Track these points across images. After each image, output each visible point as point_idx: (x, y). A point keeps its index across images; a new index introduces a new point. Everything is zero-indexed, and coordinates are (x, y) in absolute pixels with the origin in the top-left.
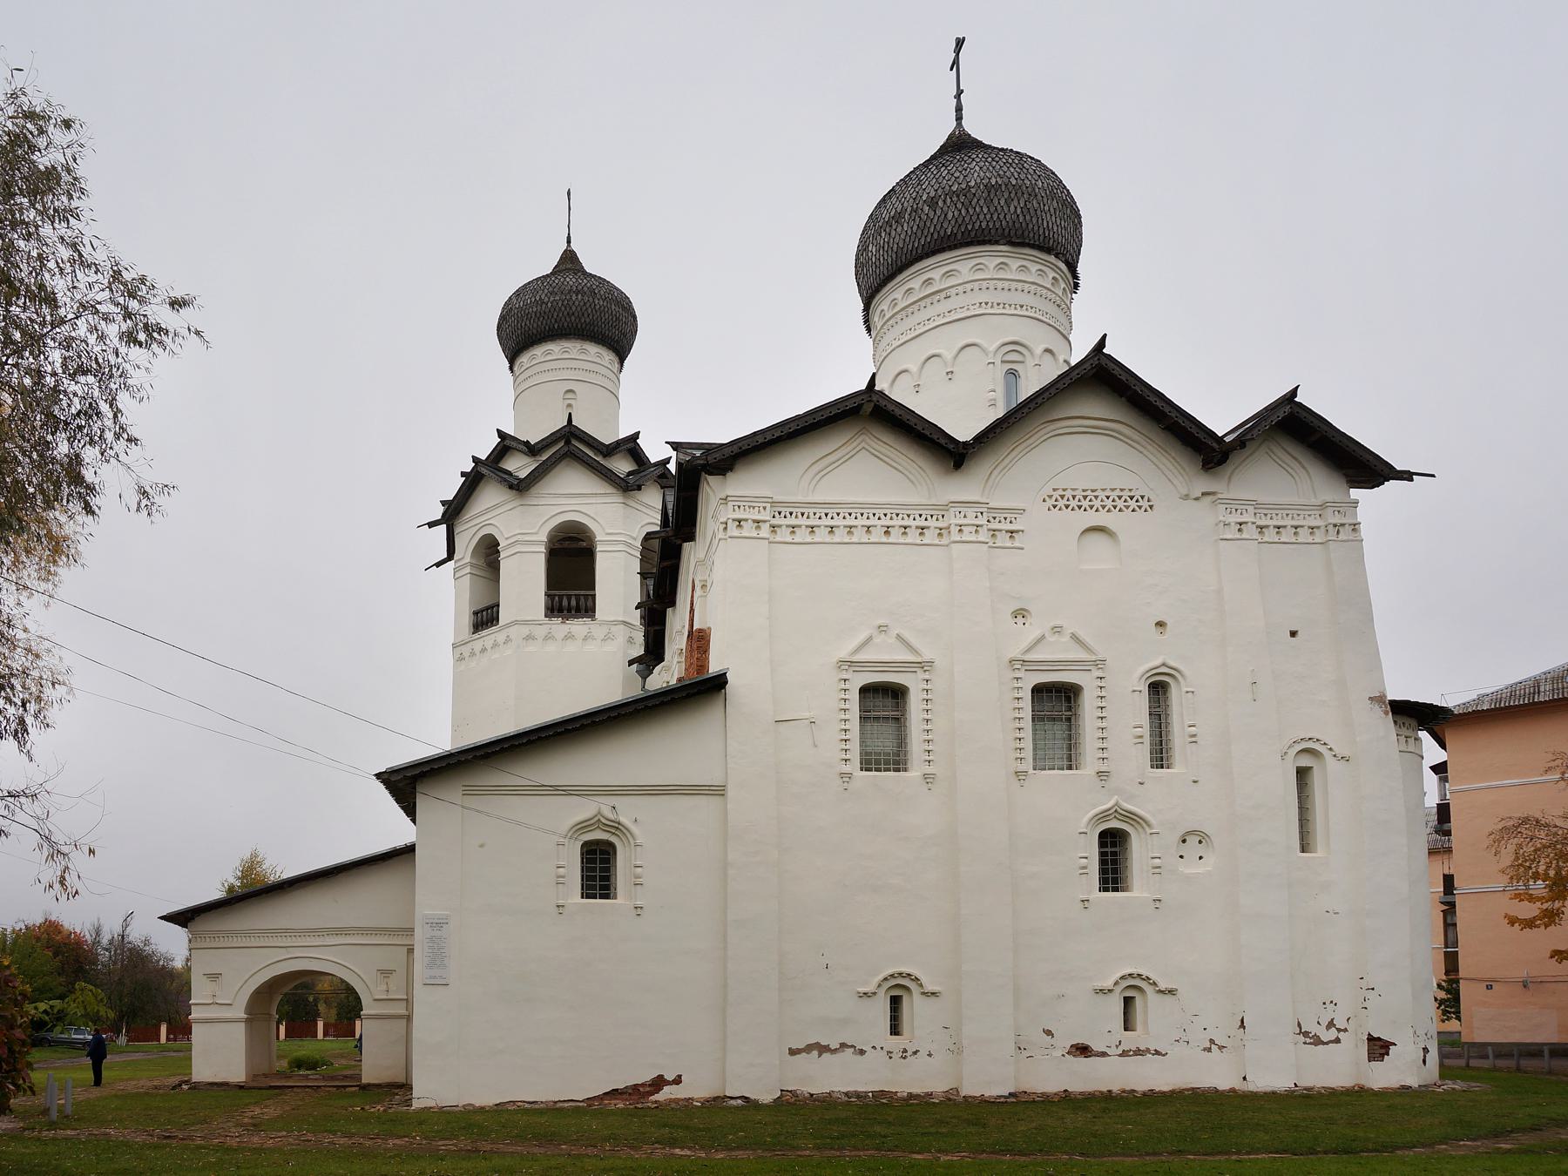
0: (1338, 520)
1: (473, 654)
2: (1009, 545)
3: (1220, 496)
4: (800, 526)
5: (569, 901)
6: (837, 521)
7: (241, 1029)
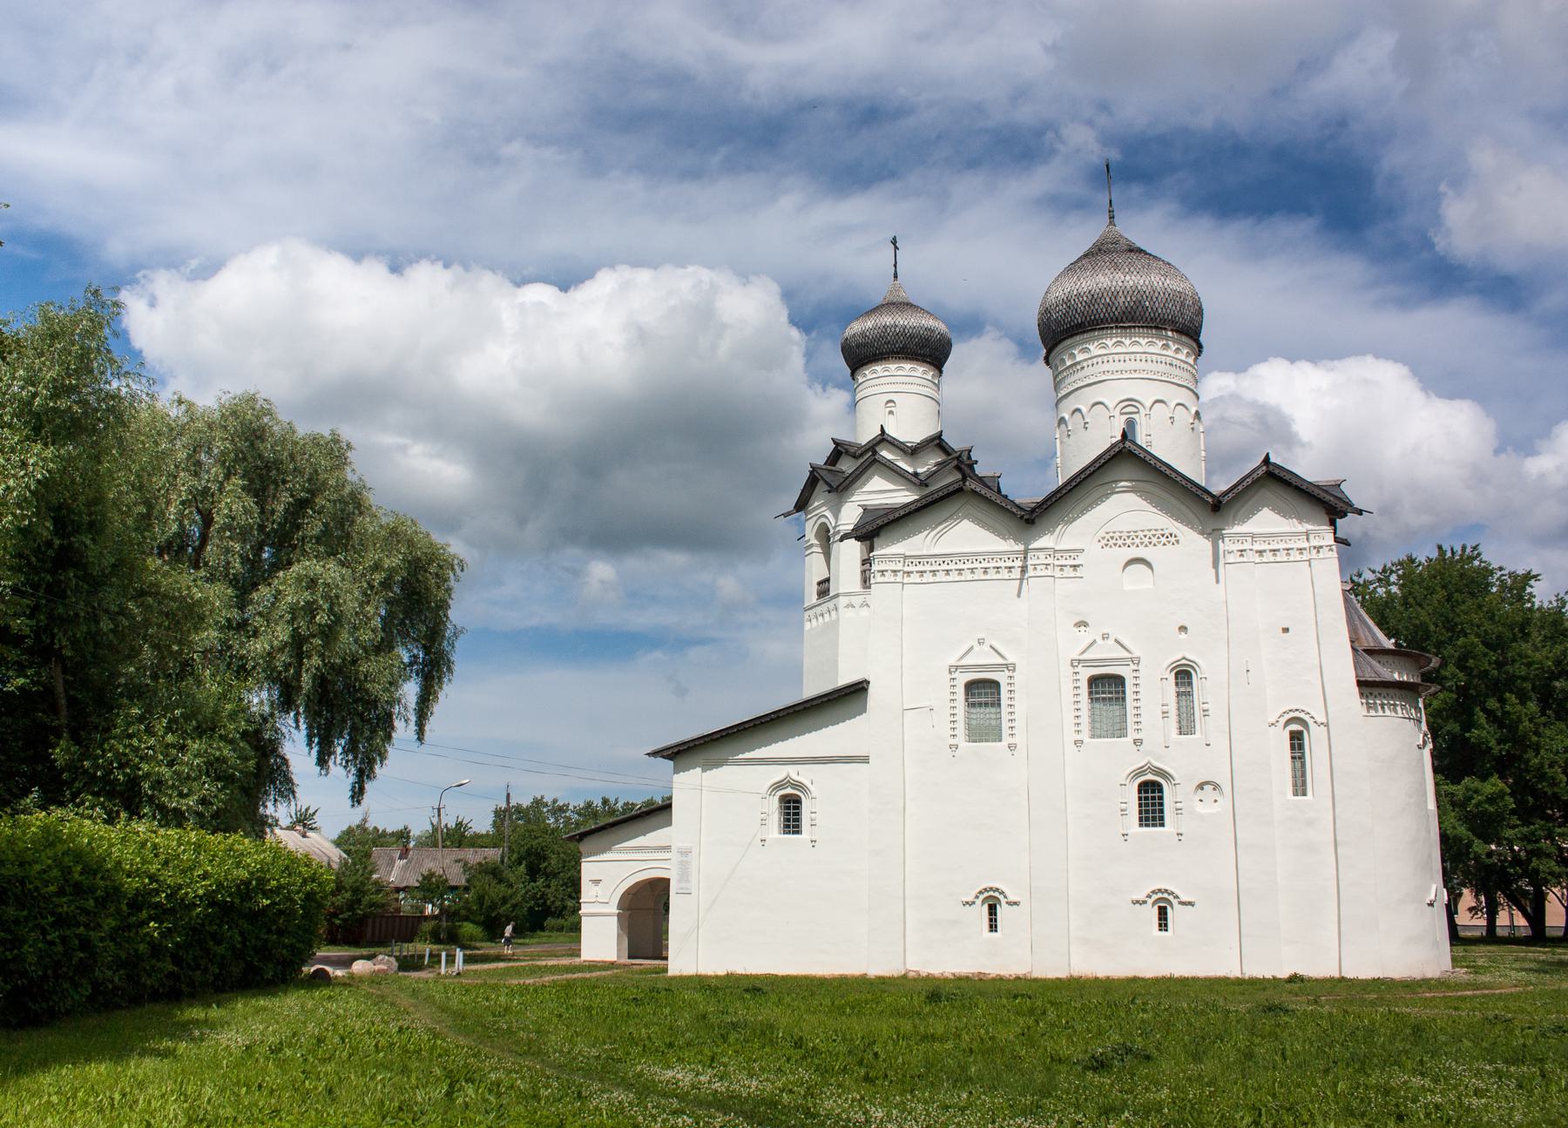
5: (770, 836)
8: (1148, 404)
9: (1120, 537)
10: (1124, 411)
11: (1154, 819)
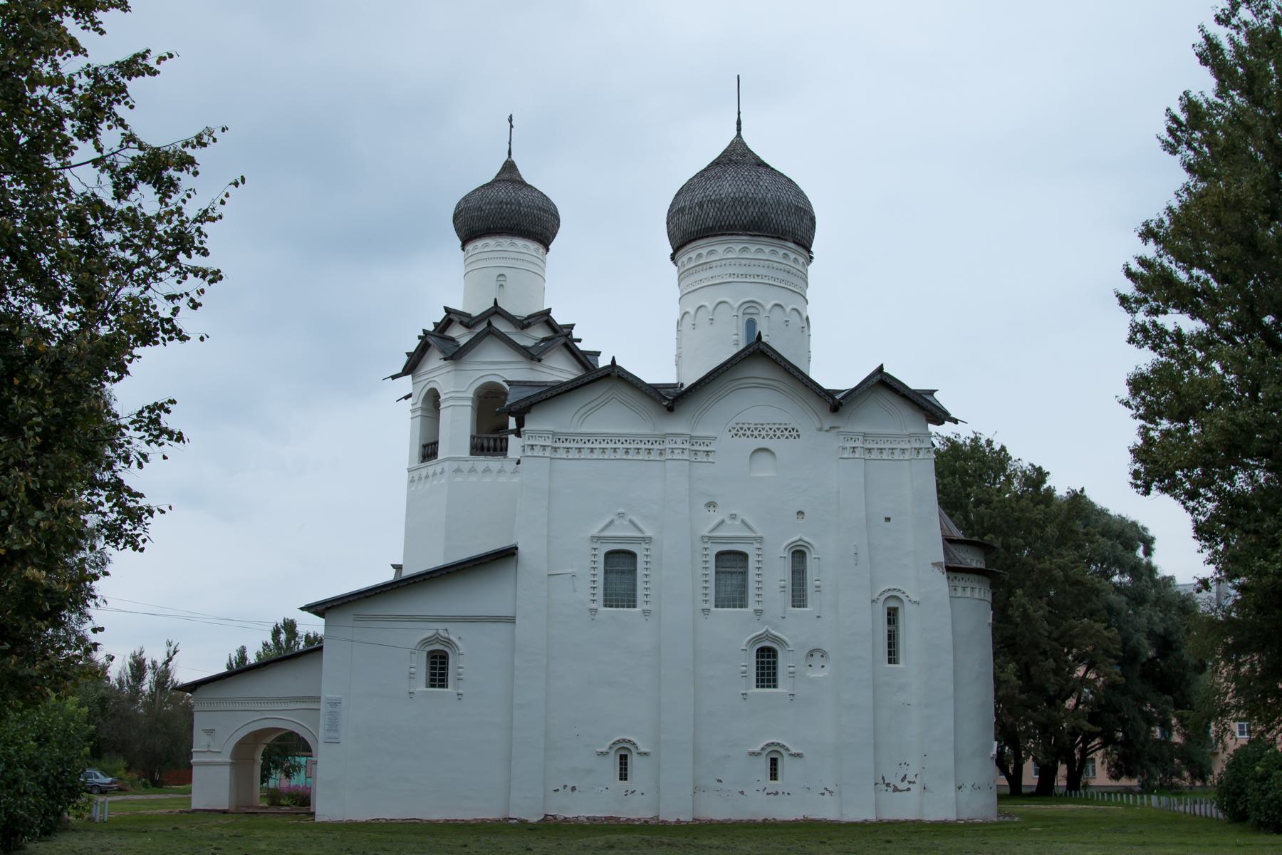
0: (917, 445)
1: (420, 478)
2: (705, 460)
3: (840, 430)
4: (572, 448)
5: (418, 689)
6: (596, 445)
7: (226, 770)
8: (768, 307)
9: (749, 429)
10: (749, 311)
11: (769, 681)
